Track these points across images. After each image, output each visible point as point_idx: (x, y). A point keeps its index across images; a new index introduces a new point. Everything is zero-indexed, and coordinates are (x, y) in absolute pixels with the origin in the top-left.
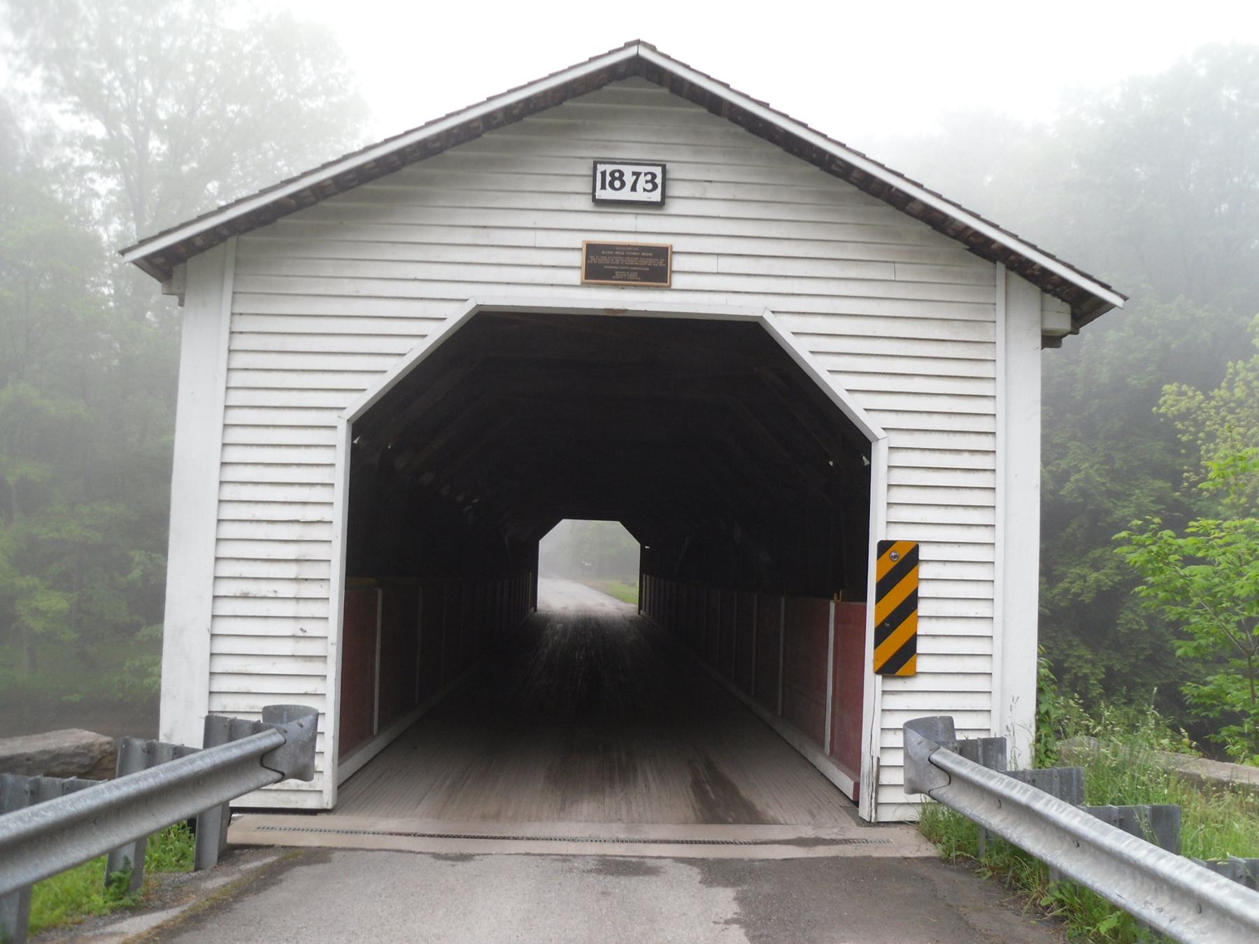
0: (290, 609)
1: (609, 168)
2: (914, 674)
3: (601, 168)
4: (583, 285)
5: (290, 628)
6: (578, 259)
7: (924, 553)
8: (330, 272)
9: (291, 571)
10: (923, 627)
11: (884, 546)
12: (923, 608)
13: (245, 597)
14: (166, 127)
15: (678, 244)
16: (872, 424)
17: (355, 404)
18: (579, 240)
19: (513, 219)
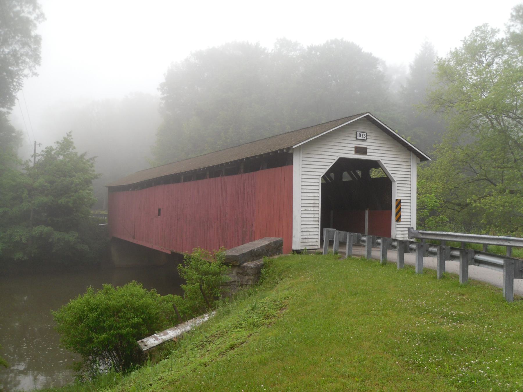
0: (312, 212)
1: (359, 133)
2: (400, 221)
3: (358, 133)
4: (355, 154)
5: (312, 216)
6: (354, 149)
7: (402, 201)
8: (317, 150)
9: (312, 205)
10: (402, 214)
11: (397, 200)
12: (402, 210)
13: (306, 210)
15: (368, 147)
16: (395, 179)
17: (322, 174)
18: (354, 146)
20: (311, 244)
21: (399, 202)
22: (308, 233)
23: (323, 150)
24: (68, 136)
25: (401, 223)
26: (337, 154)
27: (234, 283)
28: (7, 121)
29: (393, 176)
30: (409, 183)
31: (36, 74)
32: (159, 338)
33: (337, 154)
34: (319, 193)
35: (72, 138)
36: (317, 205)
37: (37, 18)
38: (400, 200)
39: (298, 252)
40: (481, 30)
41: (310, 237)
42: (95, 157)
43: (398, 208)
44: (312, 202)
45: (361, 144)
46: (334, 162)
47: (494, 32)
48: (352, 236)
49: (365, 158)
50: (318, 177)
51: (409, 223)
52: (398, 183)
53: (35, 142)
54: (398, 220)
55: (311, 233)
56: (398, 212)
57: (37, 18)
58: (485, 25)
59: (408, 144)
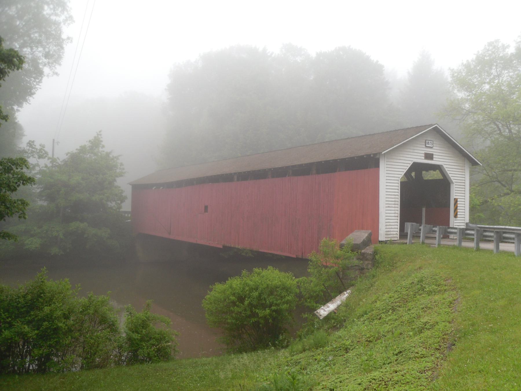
3: (427, 141)
6: (423, 155)
7: (458, 200)
9: (393, 203)
10: (458, 211)
12: (458, 208)
13: (389, 207)
14: (23, 77)
15: (434, 153)
16: (454, 181)
18: (423, 152)
19: (419, 148)
20: (392, 236)
21: (456, 201)
22: (390, 227)
23: (402, 155)
24: (98, 135)
25: (458, 219)
26: (412, 159)
27: (355, 267)
28: (16, 118)
29: (452, 178)
30: (463, 184)
31: (57, 74)
32: (326, 310)
33: (412, 159)
34: (398, 192)
35: (102, 138)
36: (397, 203)
37: (65, 21)
38: (457, 199)
39: (385, 242)
40: (493, 45)
41: (392, 230)
42: (119, 156)
43: (456, 206)
44: (393, 200)
45: (429, 151)
46: (409, 166)
47: (504, 47)
48: (441, 228)
49: (430, 163)
50: (397, 179)
51: (463, 219)
52: (455, 185)
53: (54, 140)
54: (456, 216)
55: (393, 227)
56: (456, 209)
57: (65, 21)
58: (497, 41)
59: (464, 151)
